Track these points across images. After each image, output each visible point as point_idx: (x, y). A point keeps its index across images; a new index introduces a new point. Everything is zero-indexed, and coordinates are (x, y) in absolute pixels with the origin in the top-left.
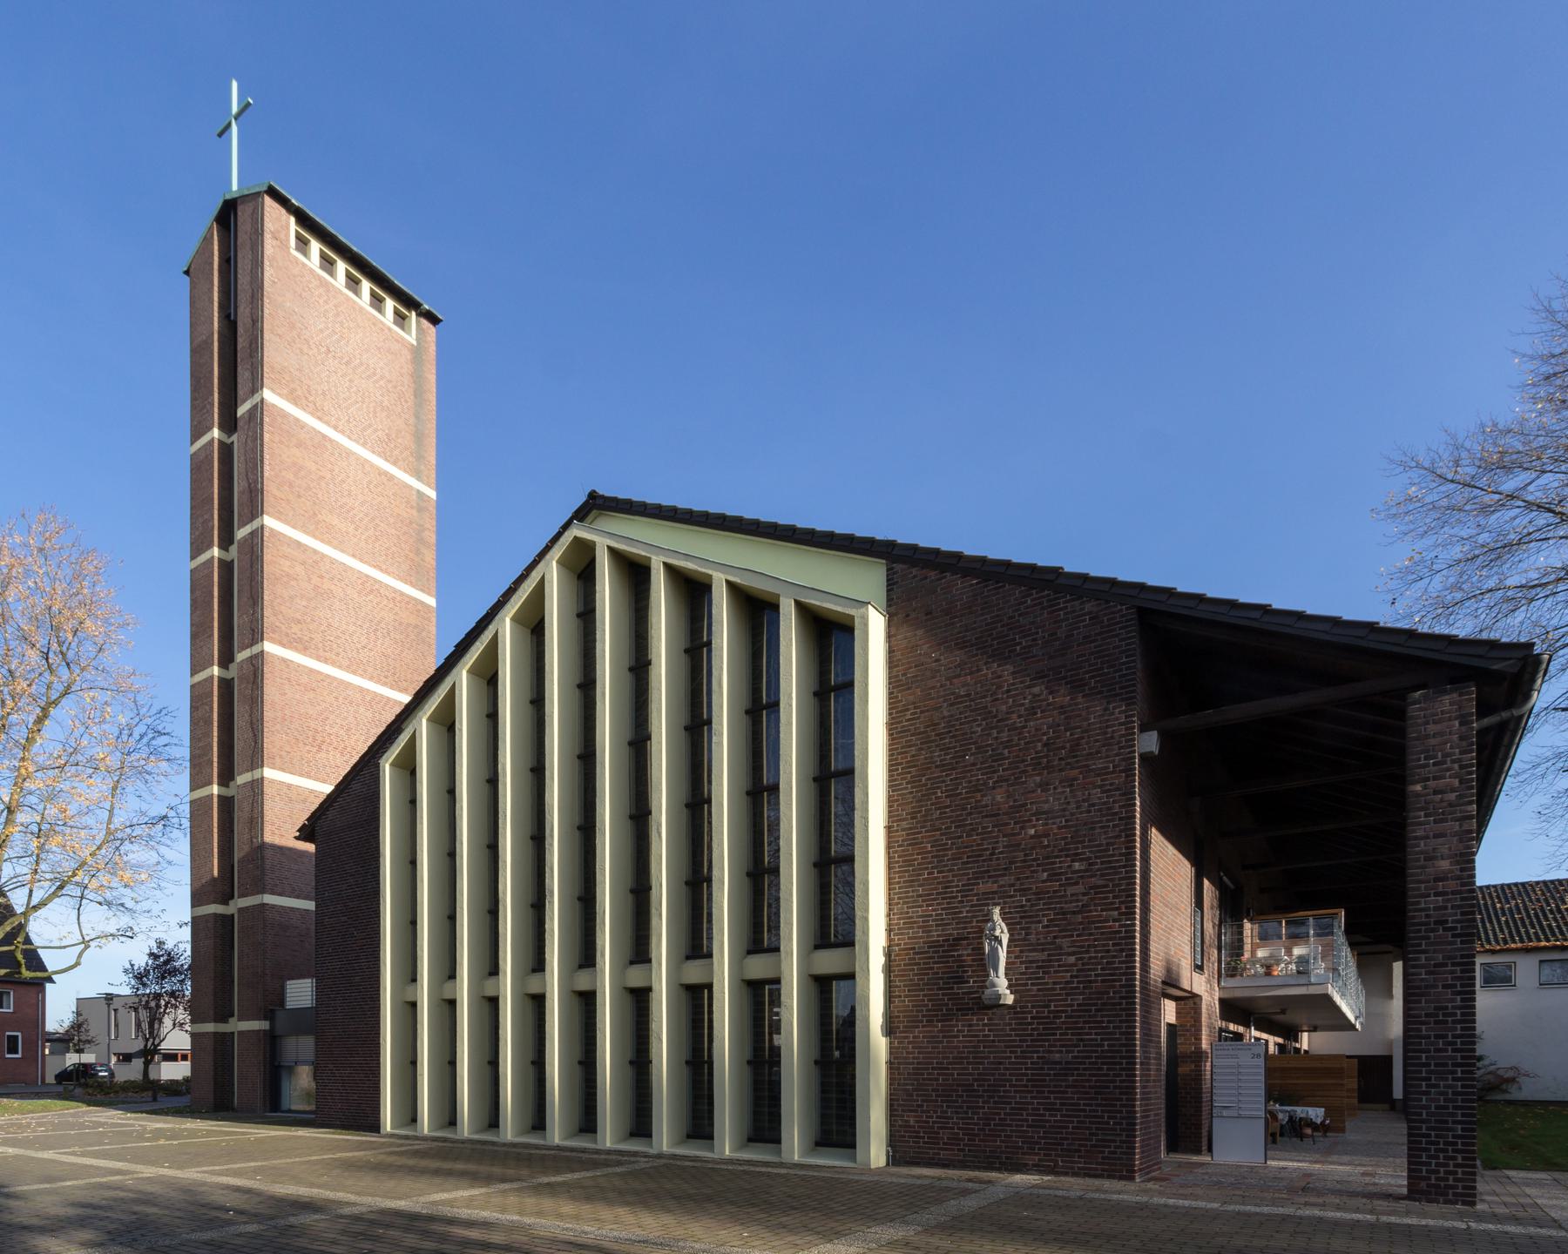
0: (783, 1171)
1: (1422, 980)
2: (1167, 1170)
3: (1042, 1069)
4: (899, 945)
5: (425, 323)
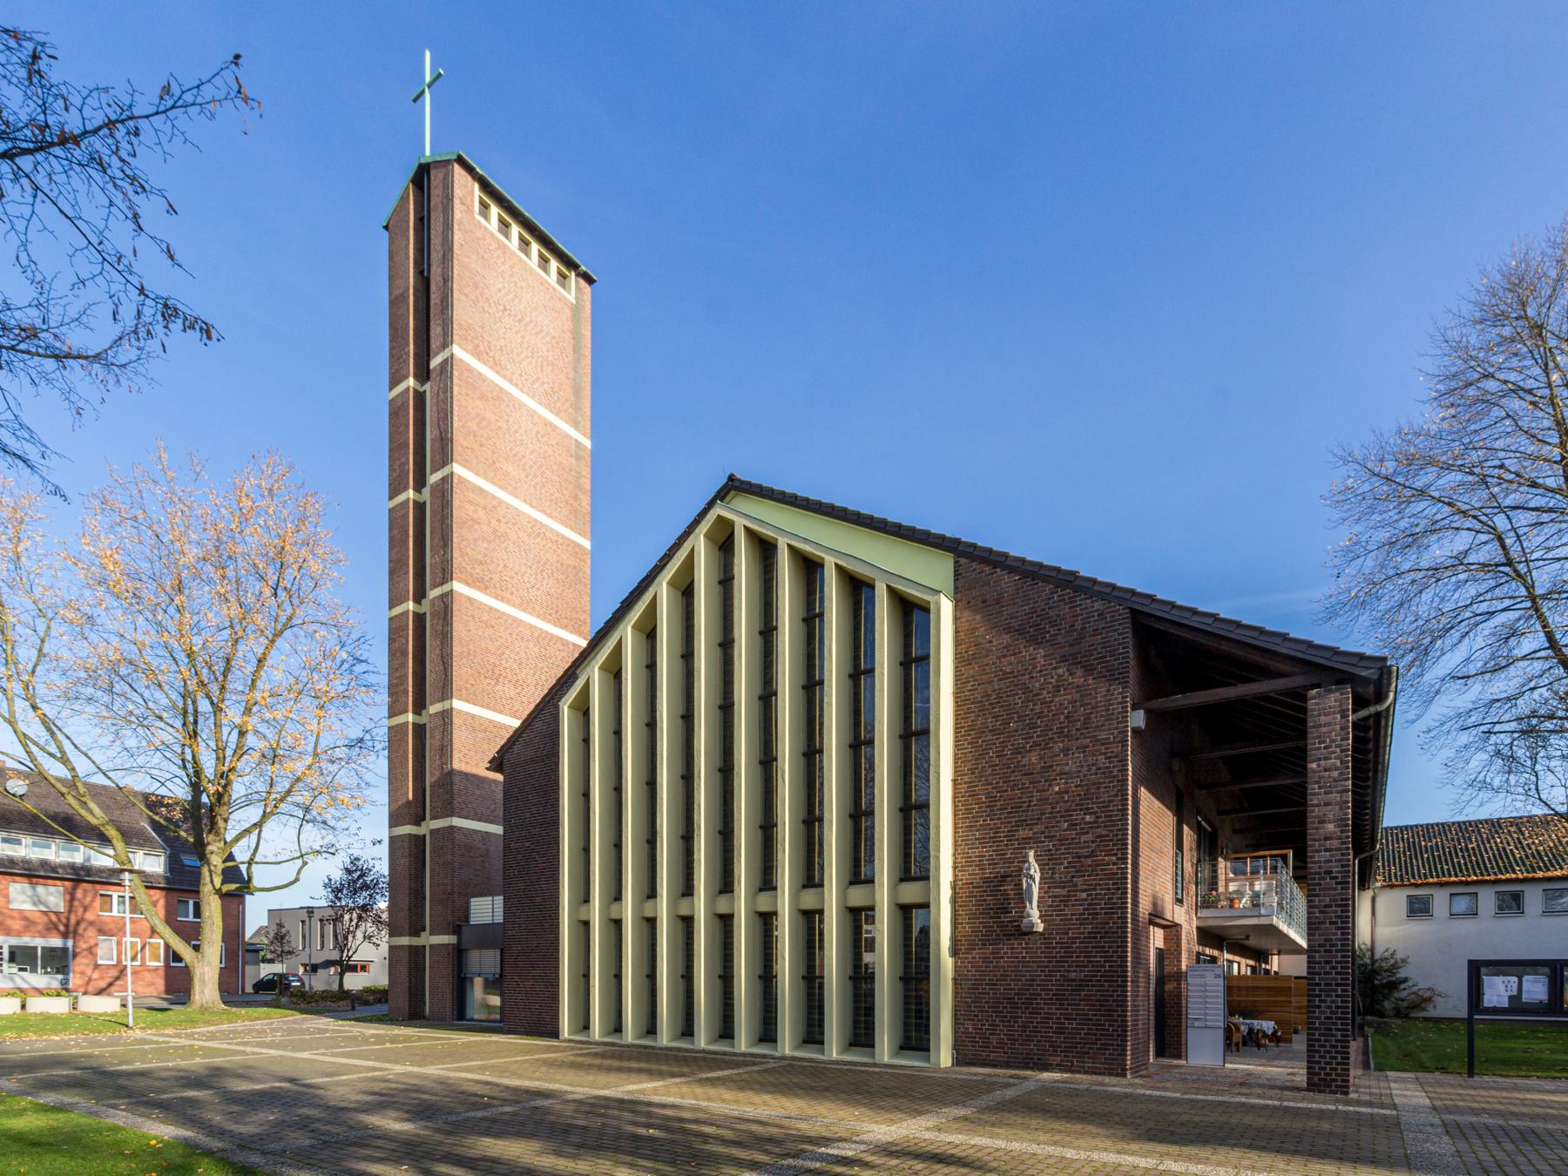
0: (878, 1070)
1: (1317, 917)
2: (1152, 1070)
3: (1063, 985)
4: (962, 880)
5: (582, 283)
